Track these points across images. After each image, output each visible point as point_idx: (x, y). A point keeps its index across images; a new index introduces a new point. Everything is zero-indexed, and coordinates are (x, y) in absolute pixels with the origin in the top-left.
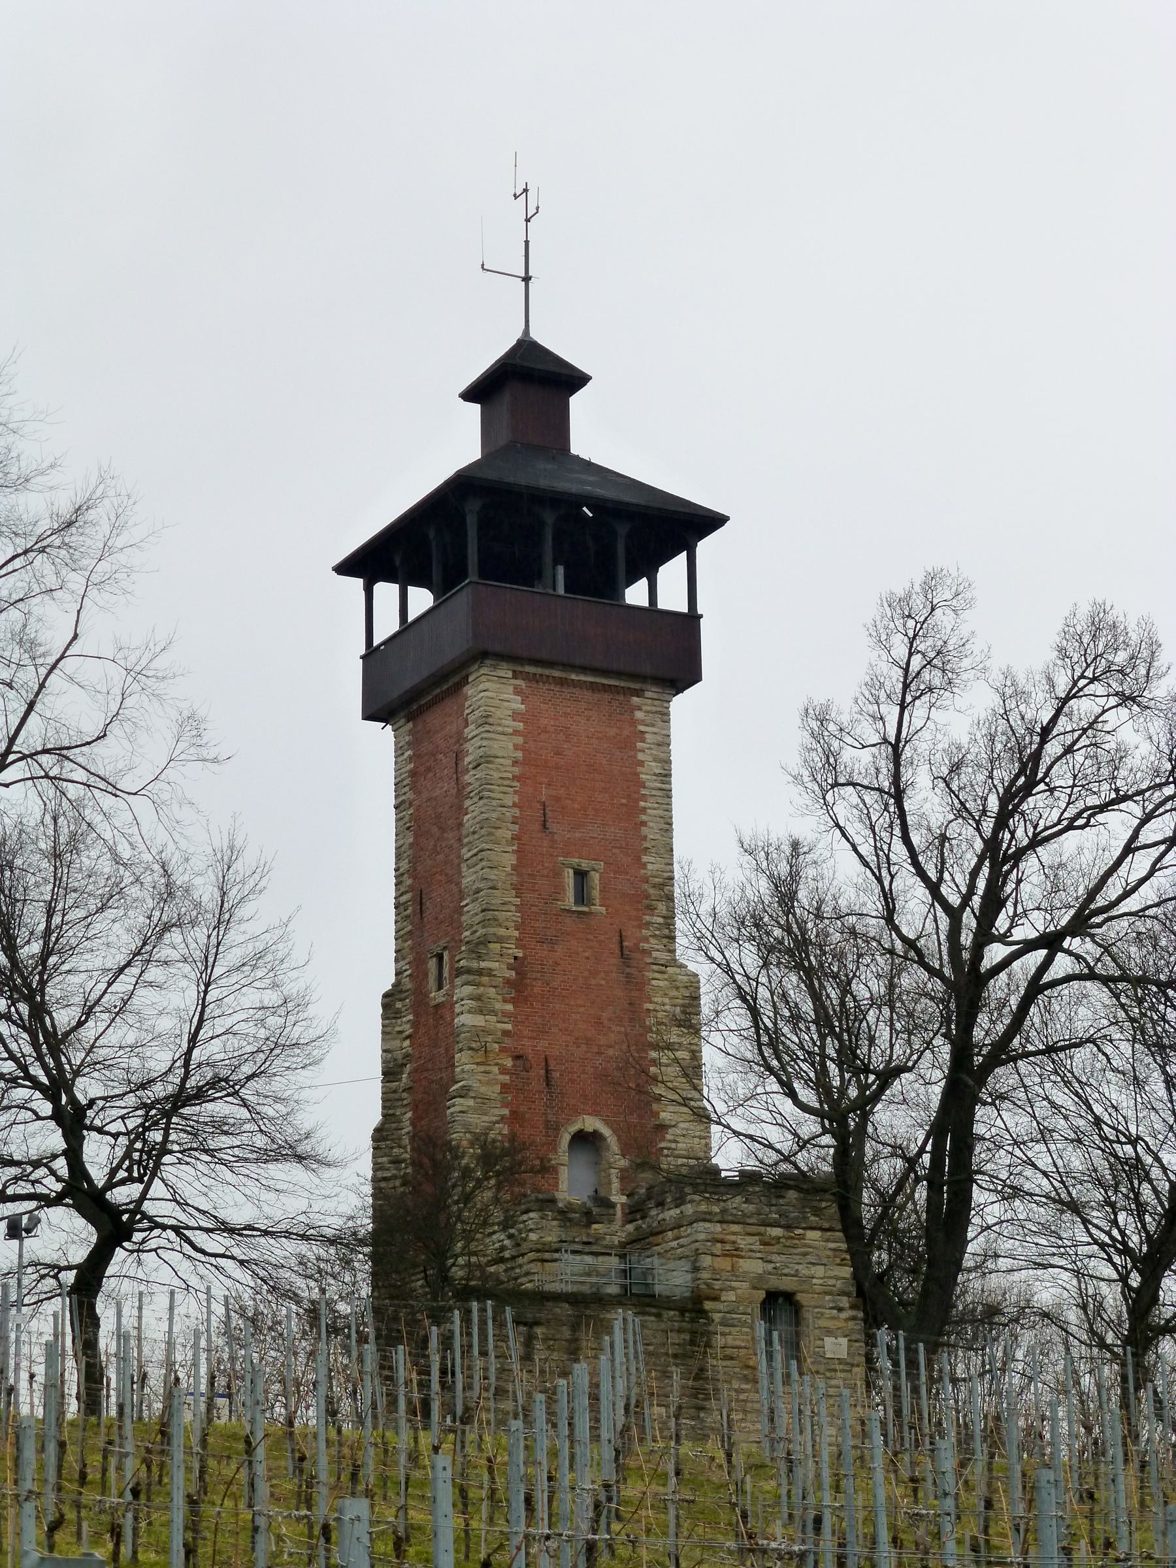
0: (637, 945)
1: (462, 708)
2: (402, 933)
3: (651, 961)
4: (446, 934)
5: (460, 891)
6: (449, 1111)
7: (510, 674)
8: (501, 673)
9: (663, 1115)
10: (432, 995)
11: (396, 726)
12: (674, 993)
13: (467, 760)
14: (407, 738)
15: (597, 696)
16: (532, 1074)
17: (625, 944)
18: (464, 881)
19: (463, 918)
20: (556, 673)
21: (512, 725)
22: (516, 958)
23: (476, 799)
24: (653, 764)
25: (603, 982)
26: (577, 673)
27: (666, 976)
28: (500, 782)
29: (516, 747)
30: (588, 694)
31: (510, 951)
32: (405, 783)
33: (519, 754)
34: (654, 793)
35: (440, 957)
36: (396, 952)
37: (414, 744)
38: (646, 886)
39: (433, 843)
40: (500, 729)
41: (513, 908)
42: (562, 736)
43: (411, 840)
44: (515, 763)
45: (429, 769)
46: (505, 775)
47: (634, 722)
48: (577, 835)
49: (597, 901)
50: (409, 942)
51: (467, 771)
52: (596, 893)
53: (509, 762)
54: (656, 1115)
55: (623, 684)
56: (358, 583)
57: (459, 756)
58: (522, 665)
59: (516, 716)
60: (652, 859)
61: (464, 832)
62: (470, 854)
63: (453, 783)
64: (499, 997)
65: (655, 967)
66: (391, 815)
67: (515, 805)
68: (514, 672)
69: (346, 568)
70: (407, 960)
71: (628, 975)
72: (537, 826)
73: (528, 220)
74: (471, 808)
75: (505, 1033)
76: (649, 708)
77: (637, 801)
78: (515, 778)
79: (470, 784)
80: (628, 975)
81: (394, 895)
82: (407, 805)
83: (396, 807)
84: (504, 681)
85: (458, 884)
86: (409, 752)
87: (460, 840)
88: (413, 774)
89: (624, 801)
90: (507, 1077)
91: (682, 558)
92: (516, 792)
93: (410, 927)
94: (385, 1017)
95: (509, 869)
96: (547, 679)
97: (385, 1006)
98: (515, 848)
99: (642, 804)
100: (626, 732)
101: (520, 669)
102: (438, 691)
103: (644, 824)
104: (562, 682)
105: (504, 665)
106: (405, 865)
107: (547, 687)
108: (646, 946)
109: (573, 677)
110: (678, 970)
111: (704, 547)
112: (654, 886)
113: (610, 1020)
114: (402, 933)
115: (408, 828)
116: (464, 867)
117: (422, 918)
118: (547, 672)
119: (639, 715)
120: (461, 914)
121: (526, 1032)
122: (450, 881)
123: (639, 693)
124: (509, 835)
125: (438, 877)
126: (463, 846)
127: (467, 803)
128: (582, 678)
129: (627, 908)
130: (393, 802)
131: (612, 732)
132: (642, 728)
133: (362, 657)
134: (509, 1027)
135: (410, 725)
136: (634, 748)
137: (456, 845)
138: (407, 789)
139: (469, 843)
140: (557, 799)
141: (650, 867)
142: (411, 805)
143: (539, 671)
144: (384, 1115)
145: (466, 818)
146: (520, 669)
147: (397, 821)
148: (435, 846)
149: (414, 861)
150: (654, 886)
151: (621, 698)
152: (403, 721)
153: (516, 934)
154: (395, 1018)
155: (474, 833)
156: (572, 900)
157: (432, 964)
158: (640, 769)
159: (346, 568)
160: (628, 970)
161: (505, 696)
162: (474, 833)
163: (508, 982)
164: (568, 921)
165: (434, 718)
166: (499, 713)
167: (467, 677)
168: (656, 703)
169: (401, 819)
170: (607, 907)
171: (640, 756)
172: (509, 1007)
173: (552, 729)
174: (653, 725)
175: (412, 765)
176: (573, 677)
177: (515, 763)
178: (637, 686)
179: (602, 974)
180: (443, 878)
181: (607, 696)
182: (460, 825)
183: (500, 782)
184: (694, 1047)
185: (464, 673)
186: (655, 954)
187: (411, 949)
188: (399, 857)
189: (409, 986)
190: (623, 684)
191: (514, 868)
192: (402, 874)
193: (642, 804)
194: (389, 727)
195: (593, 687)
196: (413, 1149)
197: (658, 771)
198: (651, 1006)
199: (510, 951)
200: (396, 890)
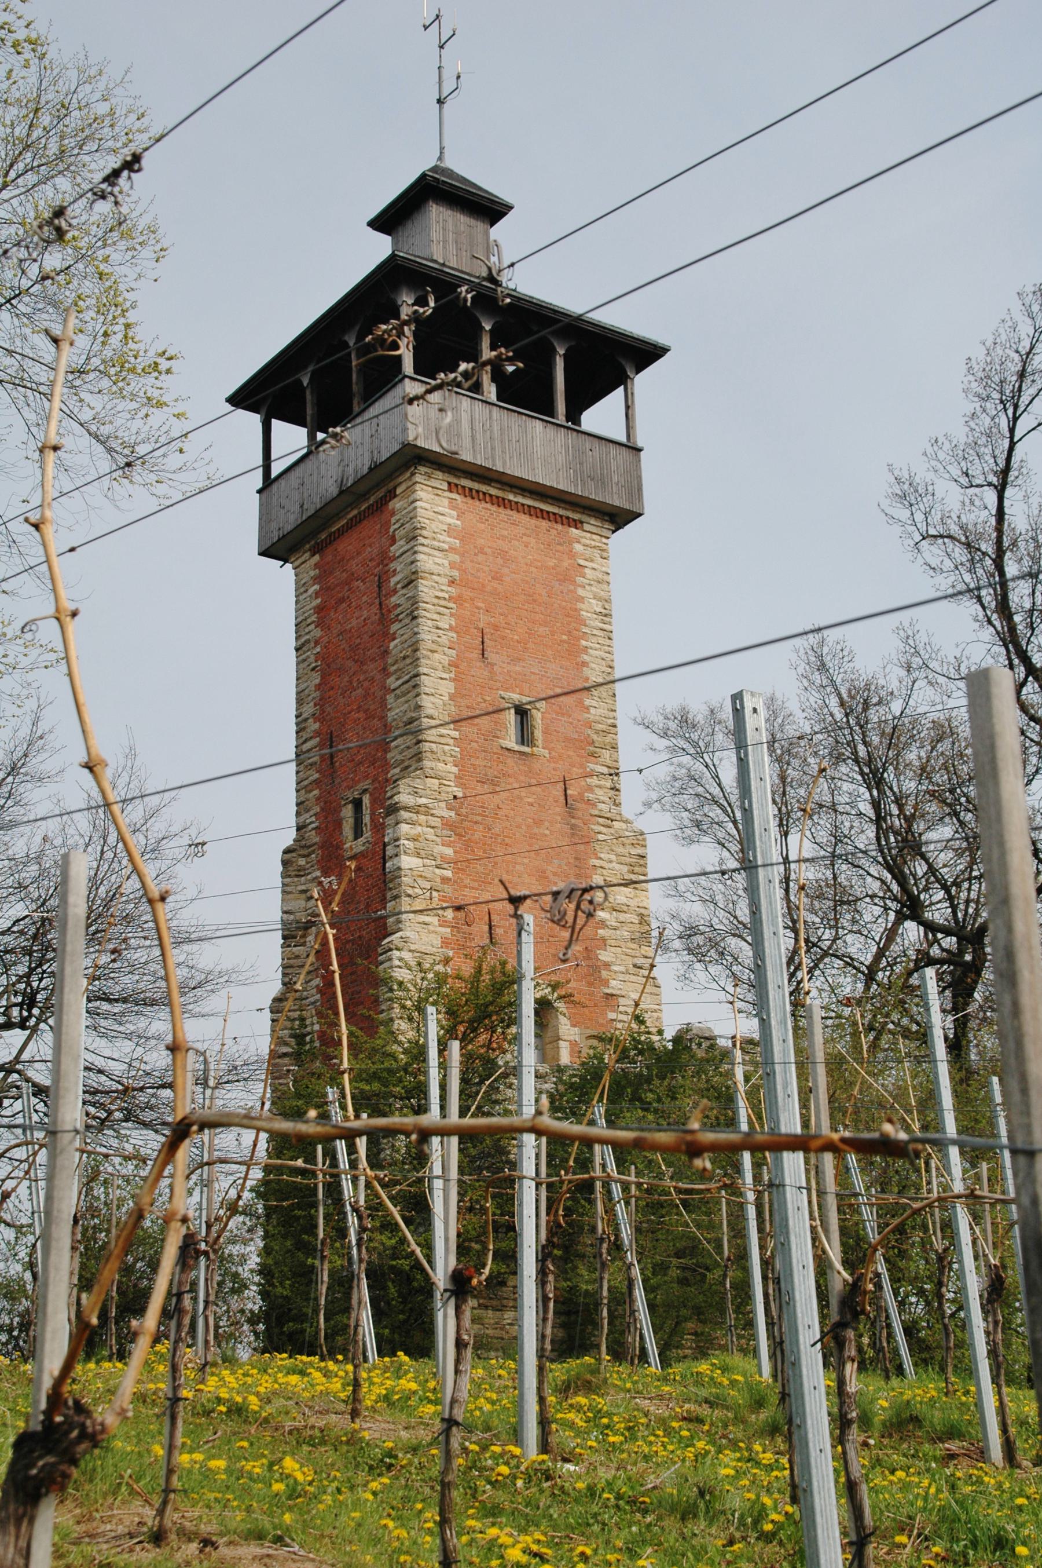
0: (581, 794)
1: (388, 524)
2: (306, 783)
3: (597, 813)
4: (367, 777)
5: (385, 726)
6: (381, 967)
7: (445, 486)
8: (437, 484)
9: (613, 983)
10: (347, 845)
11: (297, 563)
12: (621, 850)
13: (393, 581)
14: (312, 573)
15: (534, 522)
16: (474, 929)
17: (569, 792)
18: (391, 715)
19: (389, 756)
20: (493, 492)
21: (447, 541)
22: (455, 797)
23: (407, 621)
24: (594, 601)
25: (547, 832)
26: (515, 494)
27: (612, 830)
28: (436, 601)
29: (452, 565)
30: (525, 518)
31: (450, 789)
32: (309, 621)
33: (456, 573)
34: (595, 632)
35: (358, 804)
36: (298, 805)
37: (322, 576)
38: (589, 732)
39: (347, 679)
40: (436, 544)
41: (451, 742)
42: (500, 561)
43: (317, 681)
44: (452, 582)
45: (342, 600)
46: (441, 594)
47: (572, 555)
48: (517, 668)
49: (540, 743)
50: (316, 792)
51: (395, 591)
52: (538, 734)
53: (445, 581)
54: (606, 983)
55: (562, 512)
56: (254, 420)
57: (382, 581)
58: (459, 477)
59: (450, 531)
60: (594, 703)
61: (390, 661)
62: (400, 682)
63: (375, 609)
64: (438, 840)
65: (601, 820)
66: (292, 656)
67: (451, 628)
68: (449, 483)
69: (241, 399)
70: (312, 813)
71: (573, 827)
72: (476, 654)
73: (441, 47)
74: (401, 632)
75: (445, 880)
76: (588, 542)
77: (578, 639)
78: (450, 598)
79: (399, 605)
80: (573, 827)
81: (295, 743)
82: (312, 644)
83: (297, 650)
84: (439, 492)
85: (383, 718)
86: (317, 587)
87: (384, 669)
88: (319, 610)
89: (565, 637)
90: (448, 930)
91: (621, 390)
92: (452, 615)
93: (317, 776)
94: (285, 875)
95: (446, 698)
96: (484, 497)
97: (285, 863)
98: (452, 675)
99: (584, 643)
100: (566, 564)
101: (456, 481)
102: (355, 512)
103: (584, 664)
104: (501, 502)
105: (439, 474)
106: (309, 709)
107: (484, 505)
108: (591, 796)
109: (511, 497)
110: (624, 826)
111: (644, 381)
112: (597, 732)
113: (555, 874)
114: (306, 783)
115: (313, 669)
116: (390, 698)
117: (332, 763)
118: (484, 488)
119: (578, 547)
120: (386, 750)
121: (467, 882)
122: (370, 717)
123: (577, 524)
124: (446, 661)
125: (355, 715)
126: (389, 675)
127: (394, 627)
128: (520, 499)
129: (571, 753)
130: (293, 644)
131: (551, 563)
132: (582, 562)
133: (259, 492)
134: (448, 874)
135: (317, 557)
136: (574, 582)
137: (378, 676)
138: (312, 626)
139: (399, 669)
140: (496, 628)
141: (592, 711)
142: (317, 643)
143: (476, 486)
144: (284, 984)
145: (392, 644)
146: (456, 481)
147: (298, 664)
148: (351, 682)
149: (321, 703)
150: (597, 732)
151: (559, 527)
152: (307, 555)
153: (455, 770)
154: (297, 876)
155: (404, 658)
156: (513, 738)
157: (348, 812)
158: (580, 605)
159: (241, 399)
160: (573, 821)
161: (440, 509)
162: (404, 658)
163: (447, 824)
164: (510, 762)
165: (346, 546)
166: (434, 526)
167: (395, 488)
168: (595, 537)
169: (304, 660)
170: (551, 750)
171: (581, 592)
172: (449, 851)
173: (488, 551)
174: (592, 561)
175: (319, 601)
176: (511, 497)
177: (452, 582)
178: (576, 516)
179: (547, 824)
180: (361, 715)
181: (544, 524)
182: (387, 652)
183: (436, 601)
184: (642, 911)
185: (391, 485)
186: (601, 806)
187: (318, 799)
188: (300, 700)
189: (317, 839)
190: (562, 512)
191: (452, 697)
192: (306, 720)
193: (584, 643)
194: (288, 566)
195: (531, 511)
196: (536, 925)
197: (598, 610)
198: (598, 863)
199: (450, 789)
200: (297, 739)
